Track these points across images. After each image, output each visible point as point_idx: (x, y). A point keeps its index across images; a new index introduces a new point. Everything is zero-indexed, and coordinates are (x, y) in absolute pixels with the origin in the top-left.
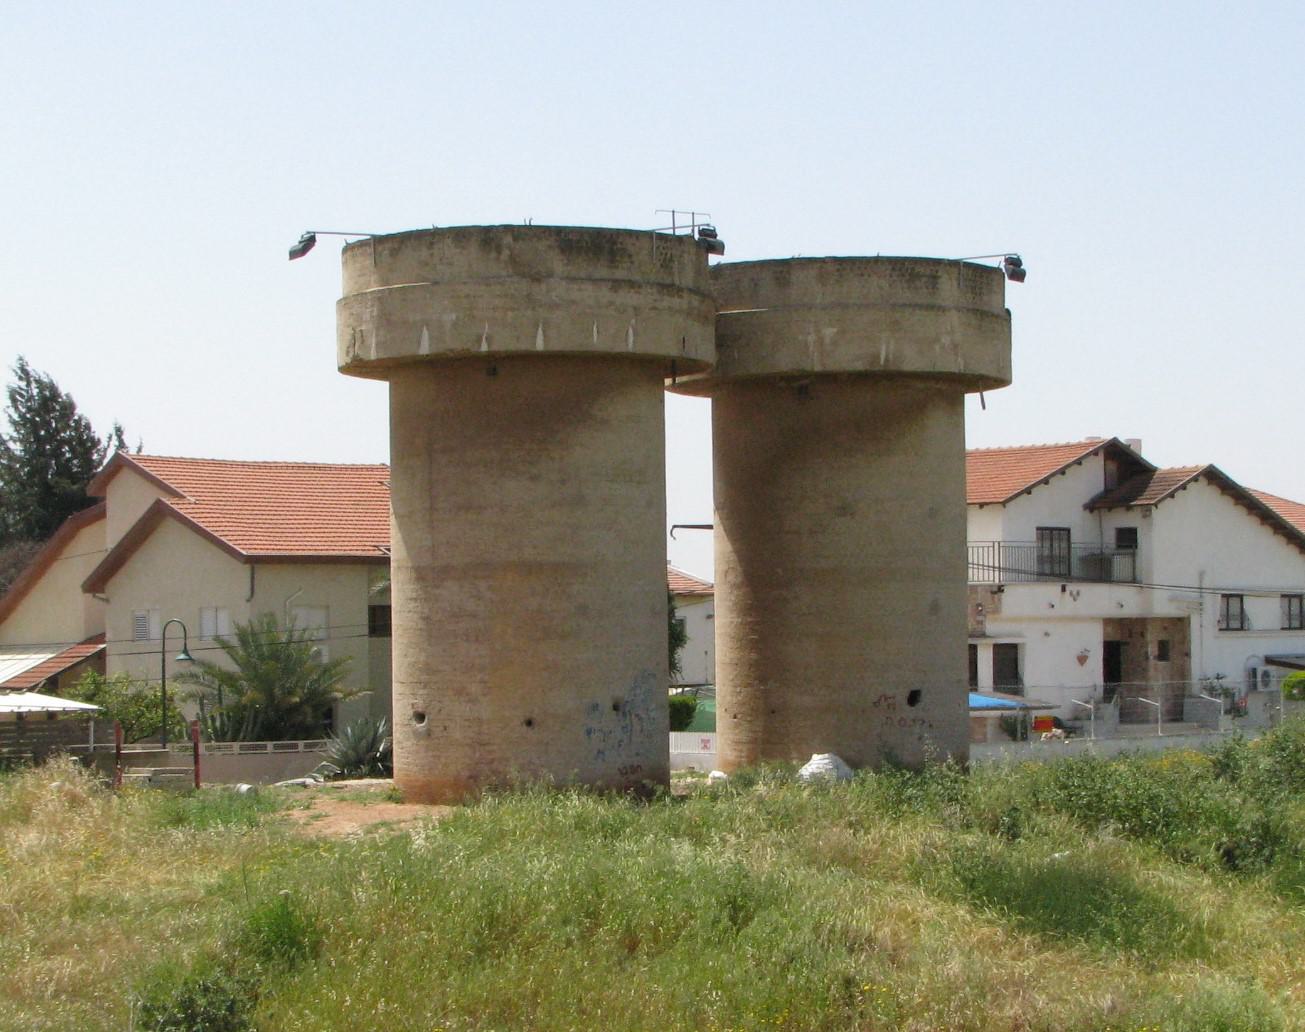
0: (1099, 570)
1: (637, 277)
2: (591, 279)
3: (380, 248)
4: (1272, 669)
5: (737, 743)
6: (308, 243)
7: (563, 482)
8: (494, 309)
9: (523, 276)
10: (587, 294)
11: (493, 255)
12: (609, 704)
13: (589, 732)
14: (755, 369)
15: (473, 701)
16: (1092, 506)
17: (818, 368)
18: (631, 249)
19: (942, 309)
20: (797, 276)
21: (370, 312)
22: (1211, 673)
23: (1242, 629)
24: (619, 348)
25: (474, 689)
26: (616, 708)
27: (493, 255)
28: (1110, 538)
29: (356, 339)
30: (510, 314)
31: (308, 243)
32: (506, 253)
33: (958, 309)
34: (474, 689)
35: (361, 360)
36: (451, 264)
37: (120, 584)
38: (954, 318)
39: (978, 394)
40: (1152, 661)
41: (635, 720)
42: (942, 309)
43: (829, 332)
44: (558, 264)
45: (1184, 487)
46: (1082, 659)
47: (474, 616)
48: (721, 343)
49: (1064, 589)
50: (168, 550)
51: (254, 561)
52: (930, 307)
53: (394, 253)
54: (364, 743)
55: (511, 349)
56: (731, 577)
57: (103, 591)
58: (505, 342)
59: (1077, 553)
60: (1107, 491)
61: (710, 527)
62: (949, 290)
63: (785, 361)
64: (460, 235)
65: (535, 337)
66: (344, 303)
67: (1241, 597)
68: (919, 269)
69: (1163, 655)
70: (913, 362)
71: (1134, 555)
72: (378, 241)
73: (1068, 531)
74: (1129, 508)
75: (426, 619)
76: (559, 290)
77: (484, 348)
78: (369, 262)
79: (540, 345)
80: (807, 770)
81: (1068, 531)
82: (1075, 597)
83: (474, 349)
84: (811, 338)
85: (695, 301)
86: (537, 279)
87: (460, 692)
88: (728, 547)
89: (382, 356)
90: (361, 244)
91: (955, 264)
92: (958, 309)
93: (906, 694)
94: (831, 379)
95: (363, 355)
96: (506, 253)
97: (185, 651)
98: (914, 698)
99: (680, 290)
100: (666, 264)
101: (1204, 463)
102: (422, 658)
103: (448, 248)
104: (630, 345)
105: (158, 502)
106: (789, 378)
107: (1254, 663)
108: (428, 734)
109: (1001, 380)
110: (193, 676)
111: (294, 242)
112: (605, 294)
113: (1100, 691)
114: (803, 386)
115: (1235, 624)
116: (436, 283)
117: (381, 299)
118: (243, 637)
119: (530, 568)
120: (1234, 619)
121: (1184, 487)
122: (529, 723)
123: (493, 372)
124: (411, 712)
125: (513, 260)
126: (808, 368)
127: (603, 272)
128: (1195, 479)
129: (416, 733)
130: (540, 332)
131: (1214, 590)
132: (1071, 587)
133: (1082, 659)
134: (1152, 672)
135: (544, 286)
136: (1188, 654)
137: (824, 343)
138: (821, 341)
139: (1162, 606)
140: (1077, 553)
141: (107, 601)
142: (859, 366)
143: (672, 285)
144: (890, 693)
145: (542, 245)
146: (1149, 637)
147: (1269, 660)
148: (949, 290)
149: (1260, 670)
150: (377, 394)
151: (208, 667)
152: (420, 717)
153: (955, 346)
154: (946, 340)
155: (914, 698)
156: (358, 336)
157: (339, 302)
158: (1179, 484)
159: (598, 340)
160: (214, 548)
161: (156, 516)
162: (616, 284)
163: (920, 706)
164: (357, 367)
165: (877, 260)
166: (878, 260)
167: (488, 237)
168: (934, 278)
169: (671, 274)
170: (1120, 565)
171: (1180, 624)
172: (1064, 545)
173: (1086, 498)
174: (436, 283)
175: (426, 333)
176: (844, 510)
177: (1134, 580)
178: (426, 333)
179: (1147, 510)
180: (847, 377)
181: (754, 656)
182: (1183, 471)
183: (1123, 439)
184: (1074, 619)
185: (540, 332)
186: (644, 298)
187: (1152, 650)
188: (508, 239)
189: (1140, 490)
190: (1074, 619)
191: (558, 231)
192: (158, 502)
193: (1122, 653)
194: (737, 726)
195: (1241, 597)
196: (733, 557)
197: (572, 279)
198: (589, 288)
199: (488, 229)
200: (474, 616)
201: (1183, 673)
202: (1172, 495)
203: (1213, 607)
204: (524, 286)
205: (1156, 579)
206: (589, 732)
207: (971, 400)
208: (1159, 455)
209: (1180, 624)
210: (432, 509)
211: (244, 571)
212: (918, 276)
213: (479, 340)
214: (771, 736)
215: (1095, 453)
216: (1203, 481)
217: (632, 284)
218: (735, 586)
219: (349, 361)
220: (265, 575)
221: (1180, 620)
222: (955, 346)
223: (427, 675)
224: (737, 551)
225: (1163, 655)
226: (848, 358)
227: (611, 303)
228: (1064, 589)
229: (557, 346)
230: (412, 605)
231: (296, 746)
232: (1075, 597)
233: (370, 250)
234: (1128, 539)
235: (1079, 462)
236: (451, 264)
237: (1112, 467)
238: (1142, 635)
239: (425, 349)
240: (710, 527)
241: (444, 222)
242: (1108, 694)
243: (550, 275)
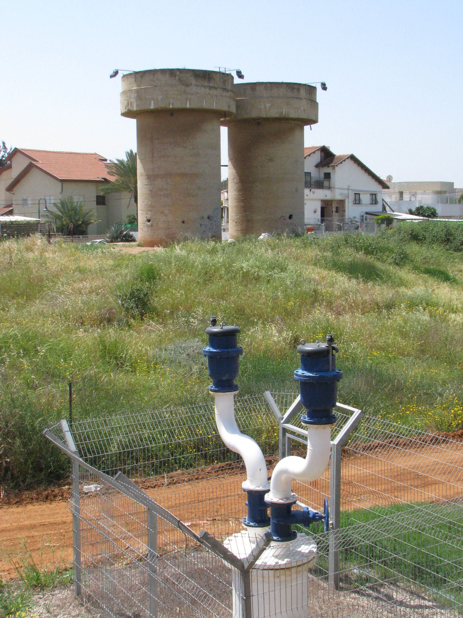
0: (319, 185)
1: (216, 86)
2: (204, 87)
3: (137, 76)
4: (368, 216)
5: (237, 230)
6: (116, 73)
7: (193, 149)
8: (174, 95)
9: (183, 85)
10: (202, 91)
11: (174, 78)
12: (207, 217)
13: (201, 225)
14: (246, 116)
15: (166, 216)
16: (317, 166)
17: (264, 116)
18: (214, 77)
19: (301, 99)
20: (258, 88)
21: (134, 95)
22: (352, 217)
23: (359, 204)
24: (211, 108)
25: (166, 212)
26: (208, 218)
27: (174, 78)
28: (322, 176)
29: (129, 104)
30: (179, 96)
31: (116, 73)
32: (177, 77)
33: (306, 99)
34: (166, 212)
35: (131, 111)
36: (160, 81)
37: (16, 189)
38: (304, 102)
39: (309, 126)
40: (334, 213)
41: (214, 222)
42: (301, 99)
43: (268, 105)
44: (193, 81)
45: (344, 161)
46: (315, 212)
47: (166, 190)
48: (238, 107)
49: (310, 190)
50: (34, 177)
51: (63, 181)
52: (297, 98)
53: (141, 77)
54: (119, 232)
55: (176, 108)
56: (235, 180)
57: (12, 191)
58: (178, 105)
59: (313, 180)
60: (321, 162)
61: (227, 166)
62: (303, 93)
63: (254, 114)
64: (163, 71)
65: (186, 103)
66: (124, 93)
67: (359, 194)
68: (295, 86)
69: (337, 212)
70: (293, 115)
71: (329, 181)
72: (136, 73)
73: (310, 173)
74: (328, 167)
75: (151, 191)
76: (194, 89)
77: (171, 107)
78: (133, 80)
79: (188, 106)
80: (261, 237)
81: (310, 173)
82: (314, 193)
83: (168, 107)
84: (262, 107)
85: (232, 93)
86: (187, 86)
87: (162, 213)
88: (234, 171)
89: (138, 109)
90: (130, 74)
91: (305, 85)
92: (297, 103)
93: (288, 216)
94: (267, 120)
95: (131, 109)
96: (177, 77)
97: (46, 208)
98: (290, 217)
99: (228, 90)
100: (224, 82)
101: (350, 153)
102: (150, 203)
103: (159, 76)
104: (214, 107)
105: (31, 163)
106: (254, 119)
107: (363, 214)
108: (152, 226)
109: (315, 121)
110: (47, 216)
111: (111, 73)
112: (207, 90)
113: (320, 220)
114: (259, 122)
115: (357, 202)
116: (156, 86)
117: (137, 91)
118: (63, 204)
119: (183, 175)
120: (357, 201)
121: (344, 161)
122: (183, 222)
123: (172, 115)
124: (146, 219)
125: (180, 80)
126: (261, 116)
127: (206, 84)
128: (348, 158)
129: (148, 226)
130: (188, 102)
131: (353, 190)
132: (312, 190)
133: (315, 212)
134: (334, 216)
135: (189, 88)
136: (344, 211)
137: (266, 109)
138: (265, 108)
139: (338, 197)
140: (313, 180)
141: (14, 194)
142: (277, 116)
143: (226, 89)
144: (284, 215)
145: (188, 75)
146: (333, 206)
147: (367, 213)
148: (303, 93)
149: (365, 216)
150: (133, 123)
151: (51, 213)
152: (149, 221)
153: (305, 110)
154: (302, 108)
155: (290, 217)
156: (130, 103)
157: (122, 93)
158: (342, 160)
159: (205, 105)
160: (49, 177)
161: (30, 167)
162: (210, 88)
163: (292, 219)
164: (128, 114)
165: (282, 83)
166: (282, 83)
167: (172, 72)
168: (299, 90)
169: (225, 85)
170: (326, 183)
171: (342, 202)
172: (309, 177)
173: (315, 164)
174: (156, 86)
175: (152, 102)
176: (271, 160)
177: (329, 188)
178: (152, 102)
179: (334, 167)
180: (267, 120)
181: (242, 204)
182: (344, 156)
183: (326, 146)
184: (312, 200)
185: (188, 102)
186: (219, 92)
187: (334, 209)
188: (178, 73)
189: (332, 161)
190: (312, 200)
191: (194, 71)
192: (31, 163)
193: (326, 209)
194: (237, 225)
195: (359, 194)
196: (236, 174)
197: (197, 86)
198: (203, 88)
199: (173, 70)
200: (166, 190)
201: (343, 216)
202: (341, 163)
203: (352, 197)
204: (183, 88)
205: (336, 186)
206: (201, 225)
207: (306, 128)
208: (337, 150)
209: (342, 202)
210: (153, 157)
211: (60, 184)
212: (294, 89)
213: (169, 104)
214: (248, 227)
215: (318, 150)
216: (350, 159)
217: (215, 88)
218: (236, 183)
219: (126, 111)
220: (66, 185)
221: (342, 200)
222: (305, 110)
223: (151, 208)
224: (237, 172)
225: (337, 212)
226: (274, 113)
227: (209, 94)
228: (310, 190)
229: (193, 106)
230: (146, 186)
231: (79, 237)
232: (314, 193)
233: (133, 76)
234: (328, 176)
235: (314, 153)
236: (160, 81)
237: (323, 154)
238: (331, 205)
239: (152, 107)
240: (227, 166)
241: (158, 68)
242: (322, 221)
243: (191, 85)
